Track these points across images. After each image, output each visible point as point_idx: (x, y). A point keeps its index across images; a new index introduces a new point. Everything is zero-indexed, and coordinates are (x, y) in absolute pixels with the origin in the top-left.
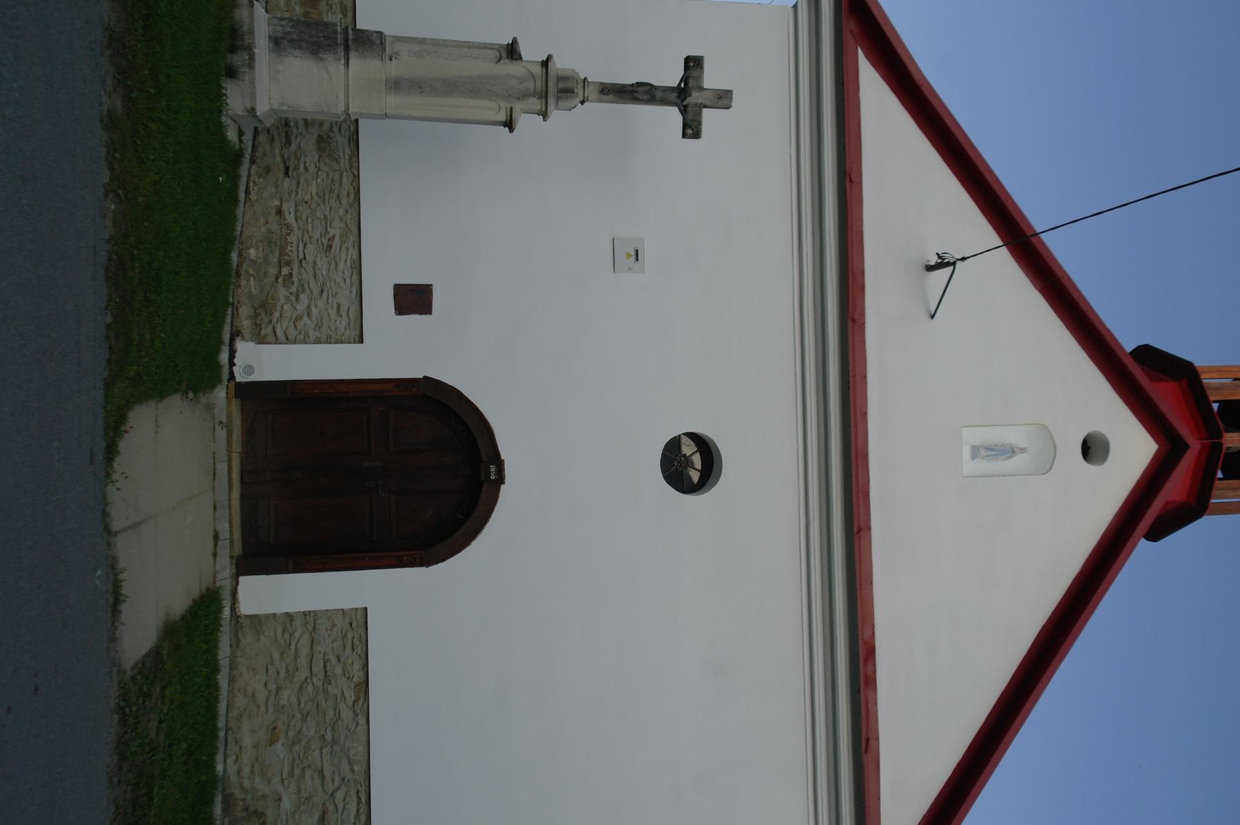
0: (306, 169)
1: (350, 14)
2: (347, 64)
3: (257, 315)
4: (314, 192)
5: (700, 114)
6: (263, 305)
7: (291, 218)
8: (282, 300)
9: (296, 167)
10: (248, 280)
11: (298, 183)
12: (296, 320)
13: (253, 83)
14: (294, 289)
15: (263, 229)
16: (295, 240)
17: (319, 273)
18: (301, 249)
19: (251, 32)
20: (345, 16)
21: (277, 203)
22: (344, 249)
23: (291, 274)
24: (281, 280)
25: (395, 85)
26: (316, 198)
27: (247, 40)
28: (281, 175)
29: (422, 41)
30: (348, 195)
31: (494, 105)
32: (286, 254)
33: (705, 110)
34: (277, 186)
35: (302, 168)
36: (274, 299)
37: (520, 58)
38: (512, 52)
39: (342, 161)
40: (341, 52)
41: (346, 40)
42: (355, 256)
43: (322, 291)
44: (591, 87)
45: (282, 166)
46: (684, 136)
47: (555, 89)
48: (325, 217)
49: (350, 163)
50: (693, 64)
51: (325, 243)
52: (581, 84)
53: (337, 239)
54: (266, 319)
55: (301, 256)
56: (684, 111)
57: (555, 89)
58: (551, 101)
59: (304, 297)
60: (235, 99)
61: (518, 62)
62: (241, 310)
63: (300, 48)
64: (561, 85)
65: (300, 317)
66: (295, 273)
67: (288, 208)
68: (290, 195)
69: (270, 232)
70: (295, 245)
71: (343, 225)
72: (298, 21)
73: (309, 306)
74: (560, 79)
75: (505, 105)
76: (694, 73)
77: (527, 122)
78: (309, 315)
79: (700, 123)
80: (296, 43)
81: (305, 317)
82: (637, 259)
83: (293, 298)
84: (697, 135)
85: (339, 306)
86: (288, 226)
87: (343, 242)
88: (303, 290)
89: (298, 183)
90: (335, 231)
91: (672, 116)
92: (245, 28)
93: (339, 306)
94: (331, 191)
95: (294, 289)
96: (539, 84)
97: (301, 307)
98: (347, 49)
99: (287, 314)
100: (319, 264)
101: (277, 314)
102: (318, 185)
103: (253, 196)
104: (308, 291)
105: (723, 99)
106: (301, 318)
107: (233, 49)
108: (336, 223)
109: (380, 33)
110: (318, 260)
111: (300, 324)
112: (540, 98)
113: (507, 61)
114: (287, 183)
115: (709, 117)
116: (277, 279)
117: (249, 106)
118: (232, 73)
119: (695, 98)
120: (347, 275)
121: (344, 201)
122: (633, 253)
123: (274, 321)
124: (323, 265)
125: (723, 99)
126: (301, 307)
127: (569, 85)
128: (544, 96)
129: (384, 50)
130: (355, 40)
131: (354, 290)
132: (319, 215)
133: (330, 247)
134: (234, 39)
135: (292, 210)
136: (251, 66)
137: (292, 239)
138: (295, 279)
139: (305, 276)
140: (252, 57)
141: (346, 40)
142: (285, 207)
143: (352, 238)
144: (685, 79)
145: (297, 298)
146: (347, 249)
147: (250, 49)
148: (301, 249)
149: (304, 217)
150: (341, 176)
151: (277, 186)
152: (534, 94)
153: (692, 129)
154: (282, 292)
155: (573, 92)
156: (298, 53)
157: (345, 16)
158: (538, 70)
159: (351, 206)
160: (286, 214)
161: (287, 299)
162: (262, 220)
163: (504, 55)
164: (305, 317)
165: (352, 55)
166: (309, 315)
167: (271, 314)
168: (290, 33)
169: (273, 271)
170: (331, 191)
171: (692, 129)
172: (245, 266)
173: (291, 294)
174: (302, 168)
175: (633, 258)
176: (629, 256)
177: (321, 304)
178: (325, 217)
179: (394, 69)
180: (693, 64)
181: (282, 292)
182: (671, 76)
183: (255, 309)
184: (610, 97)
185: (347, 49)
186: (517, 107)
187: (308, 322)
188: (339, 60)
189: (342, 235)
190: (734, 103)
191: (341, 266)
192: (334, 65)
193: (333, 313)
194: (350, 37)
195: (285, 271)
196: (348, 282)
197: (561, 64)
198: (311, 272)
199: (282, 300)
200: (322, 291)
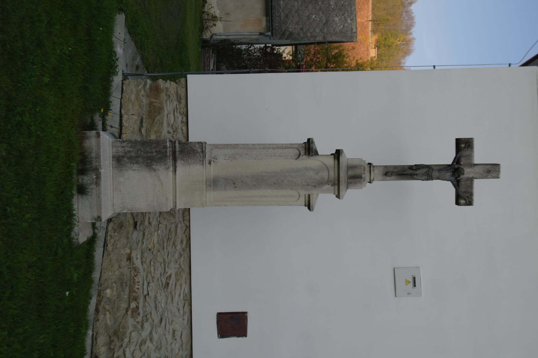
0: (150, 223)
1: (183, 101)
2: (175, 171)
3: (111, 341)
4: (156, 241)
5: (471, 186)
6: (116, 333)
7: (138, 263)
8: (131, 328)
9: (142, 223)
10: (105, 314)
11: (144, 234)
12: (141, 345)
13: (99, 196)
14: (139, 319)
15: (117, 273)
16: (141, 280)
17: (159, 305)
18: (145, 287)
19: (98, 157)
20: (180, 103)
21: (128, 251)
22: (178, 286)
23: (137, 307)
24: (129, 313)
25: (214, 183)
26: (157, 246)
27: (94, 164)
28: (131, 228)
29: (235, 146)
30: (182, 242)
31: (295, 193)
32: (134, 292)
33: (475, 180)
34: (128, 238)
35: (146, 223)
36: (124, 328)
37: (316, 153)
38: (309, 148)
39: (177, 215)
40: (170, 162)
41: (174, 152)
42: (187, 290)
43: (161, 319)
44: (376, 171)
45: (132, 222)
46: (457, 203)
47: (345, 175)
48: (164, 260)
49: (183, 217)
50: (463, 146)
51: (164, 281)
52: (367, 168)
53: (173, 277)
54: (118, 344)
55: (145, 292)
56: (457, 184)
57: (345, 175)
58: (342, 187)
59: (147, 325)
60: (83, 210)
61: (314, 157)
62: (99, 340)
63: (137, 163)
64: (351, 173)
65: (143, 342)
66: (141, 306)
67: (136, 255)
68: (138, 244)
69: (122, 274)
70: (141, 283)
71: (177, 266)
72: (136, 142)
73: (151, 333)
74: (350, 167)
75: (303, 193)
76: (465, 153)
77: (324, 199)
78: (151, 340)
79: (471, 194)
80: (134, 159)
81: (148, 342)
82: (415, 285)
83: (139, 326)
84: (458, 141)
85: (174, 331)
86: (135, 269)
87: (177, 280)
88: (147, 320)
89: (144, 234)
90: (172, 271)
91: (445, 189)
92: (93, 155)
93: (174, 331)
94: (169, 239)
95: (139, 319)
96: (332, 174)
97: (145, 334)
98: (175, 159)
99: (134, 340)
100: (159, 298)
101: (126, 340)
102: (159, 236)
103: (110, 247)
104: (150, 320)
105: (492, 170)
106: (145, 342)
107: (82, 172)
108: (172, 265)
109: (201, 143)
110: (158, 295)
111: (144, 348)
112: (334, 185)
113: (305, 157)
114: (136, 235)
115: (481, 187)
116: (127, 311)
117: (96, 215)
118: (82, 190)
119: (468, 172)
120: (181, 305)
121: (179, 247)
122: (411, 280)
123: (124, 346)
124: (162, 299)
125: (492, 170)
126: (145, 334)
127: (357, 172)
128: (337, 183)
129: (204, 156)
130: (181, 152)
131: (186, 317)
132: (160, 259)
133: (168, 284)
134: (86, 164)
135: (139, 257)
136: (97, 183)
137: (139, 279)
138: (141, 311)
139: (148, 309)
140: (98, 177)
141: (174, 152)
142: (134, 255)
143: (185, 276)
144: (457, 160)
145: (142, 326)
146: (181, 285)
147: (97, 170)
148: (145, 287)
149: (148, 261)
150: (176, 227)
151: (128, 238)
152: (328, 182)
153: (464, 197)
154: (131, 322)
155: (361, 178)
156: (136, 166)
157: (180, 103)
158: (331, 162)
159: (184, 250)
160: (135, 260)
161: (135, 327)
162: (116, 266)
163: (302, 152)
164: (148, 342)
165: (179, 163)
166: (151, 340)
167: (122, 340)
168: (129, 152)
169: (124, 305)
170: (169, 239)
171: (464, 197)
172: (102, 303)
173: (138, 322)
174: (146, 223)
175: (411, 284)
176: (408, 282)
177: (160, 331)
178: (164, 260)
179: (213, 171)
180: (463, 146)
181: (131, 322)
182: (447, 157)
183: (110, 337)
184: (393, 177)
185: (175, 159)
186: (313, 193)
187: (151, 345)
188: (168, 169)
189: (177, 275)
190: (502, 174)
191: (176, 299)
192: (164, 173)
193: (169, 337)
194: (178, 149)
195: (133, 305)
196: (181, 311)
197: (350, 155)
198: (153, 305)
199: (131, 328)
200: (161, 319)
